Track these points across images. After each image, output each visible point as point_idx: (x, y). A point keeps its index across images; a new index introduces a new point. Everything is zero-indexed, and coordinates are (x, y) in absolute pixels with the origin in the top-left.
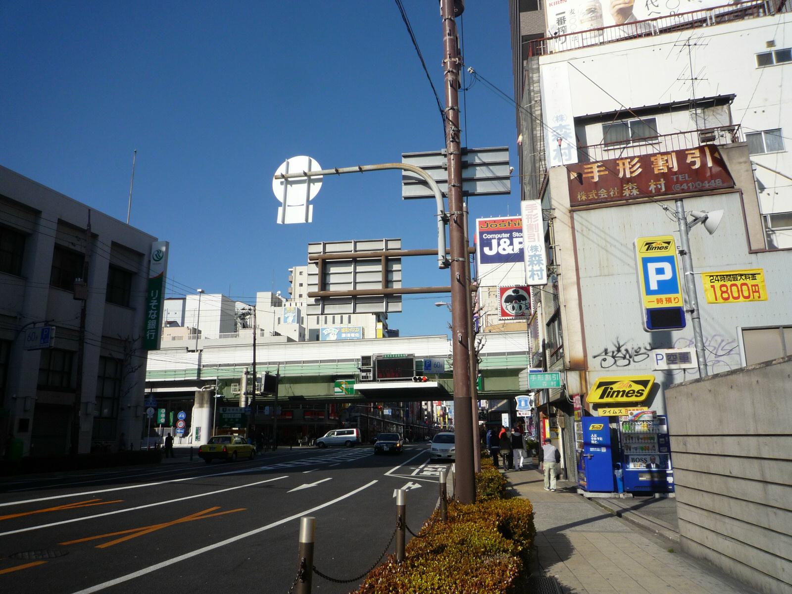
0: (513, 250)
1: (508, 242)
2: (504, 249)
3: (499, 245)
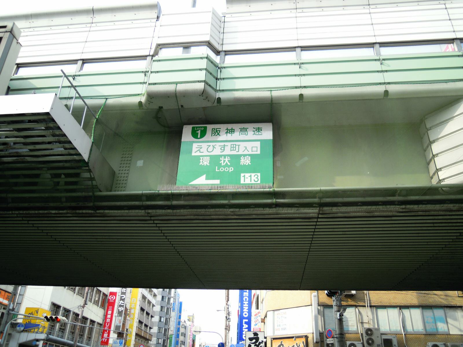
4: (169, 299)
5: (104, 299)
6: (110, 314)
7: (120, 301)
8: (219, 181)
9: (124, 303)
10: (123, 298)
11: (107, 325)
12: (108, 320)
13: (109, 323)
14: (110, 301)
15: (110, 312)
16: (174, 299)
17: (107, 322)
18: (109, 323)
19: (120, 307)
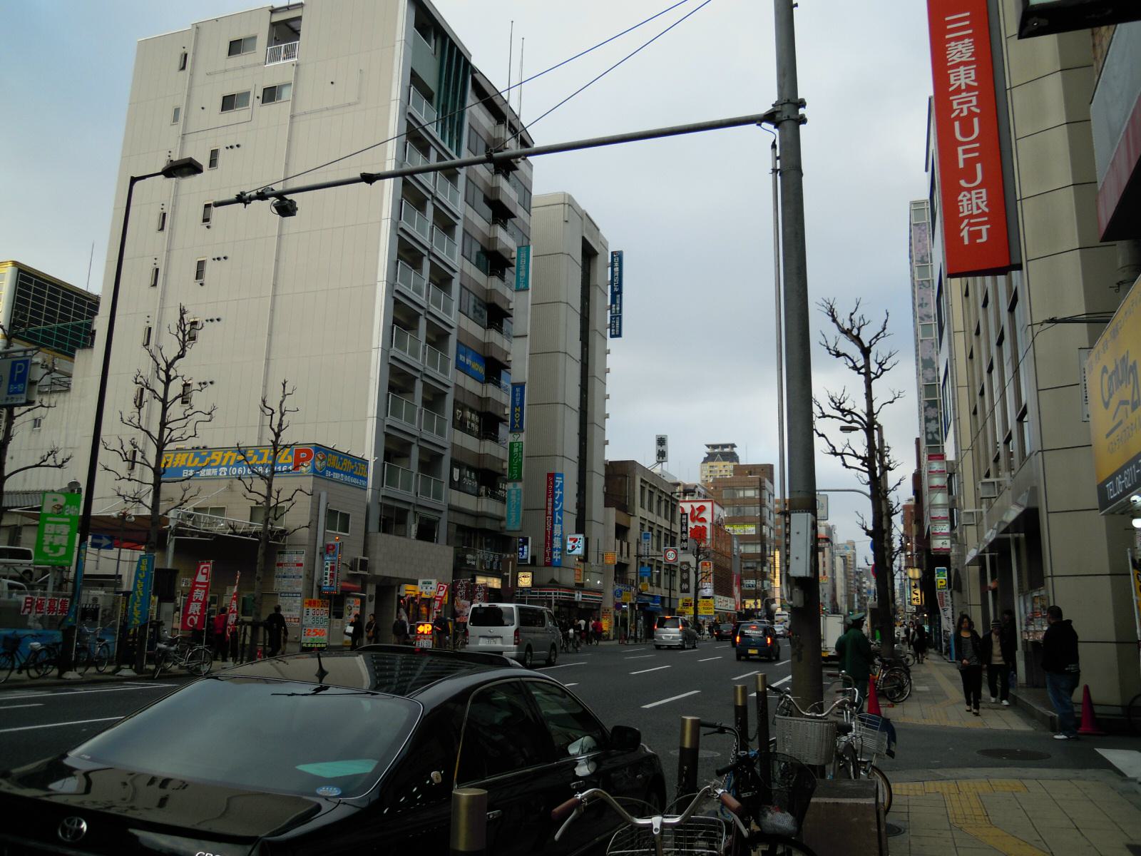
6: (965, 64)
11: (967, 131)
13: (976, 120)
18: (976, 120)
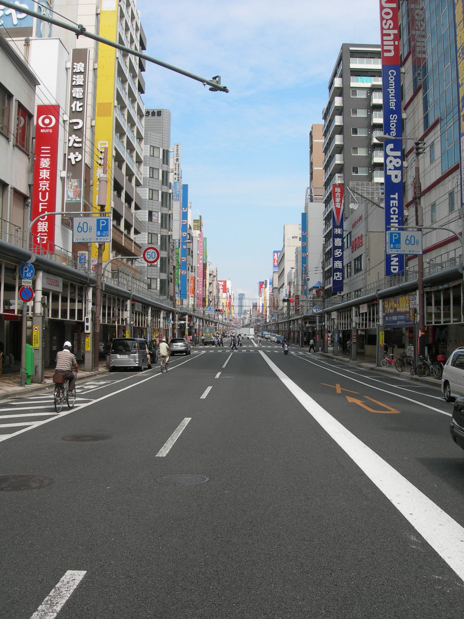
0: (390, 169)
1: (398, 165)
2: (391, 162)
3: (395, 157)
4: (165, 174)
5: (24, 128)
7: (70, 135)
8: (391, 197)
9: (80, 140)
10: (75, 128)
11: (44, 197)
12: (44, 186)
13: (47, 193)
14: (42, 131)
15: (45, 163)
16: (175, 174)
17: (41, 191)
18: (47, 193)
19: (72, 154)
